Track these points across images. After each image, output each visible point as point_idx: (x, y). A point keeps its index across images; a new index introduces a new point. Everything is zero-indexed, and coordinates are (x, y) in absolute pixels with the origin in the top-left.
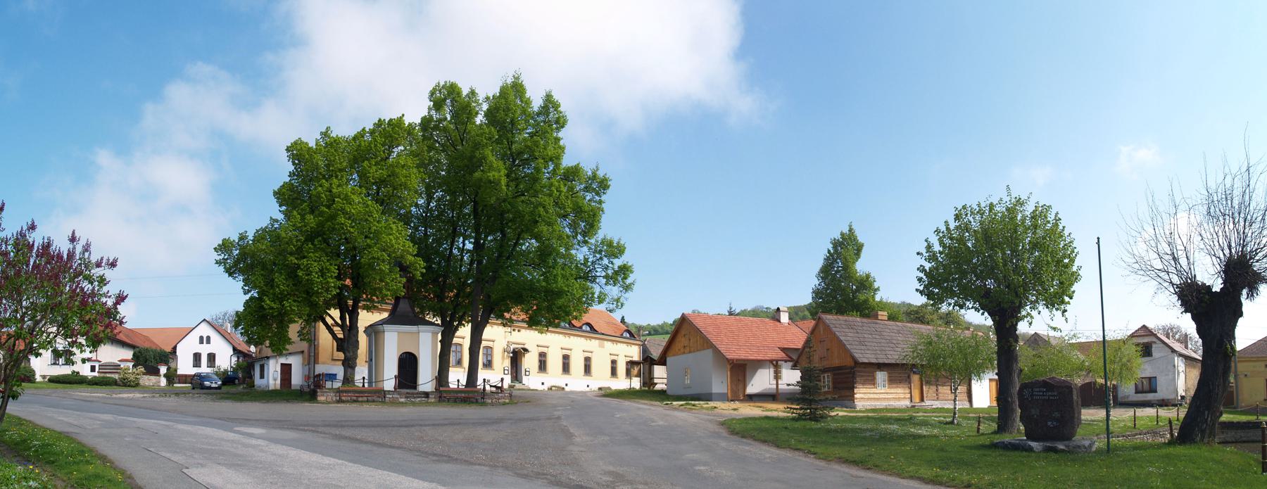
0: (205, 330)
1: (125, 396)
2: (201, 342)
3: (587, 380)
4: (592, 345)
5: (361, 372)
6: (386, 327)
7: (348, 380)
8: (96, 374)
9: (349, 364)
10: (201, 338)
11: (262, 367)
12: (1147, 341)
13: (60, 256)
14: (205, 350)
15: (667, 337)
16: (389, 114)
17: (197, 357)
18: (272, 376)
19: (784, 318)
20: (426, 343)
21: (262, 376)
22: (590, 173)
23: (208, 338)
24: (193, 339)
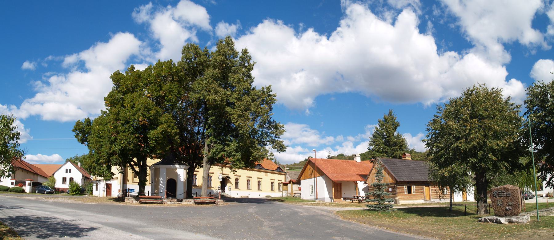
0: (69, 166)
1: (30, 198)
2: (67, 172)
3: (259, 192)
4: (262, 175)
5: (148, 188)
6: (161, 166)
7: (141, 191)
8: (13, 186)
9: (142, 184)
10: (67, 170)
11: (97, 185)
12: (188, 40)
13: (528, 107)
14: (68, 176)
15: (300, 170)
16: (181, 49)
17: (64, 179)
18: (99, 191)
19: (358, 159)
20: (181, 172)
21: (97, 190)
22: (383, 120)
23: (70, 170)
24: (63, 169)
